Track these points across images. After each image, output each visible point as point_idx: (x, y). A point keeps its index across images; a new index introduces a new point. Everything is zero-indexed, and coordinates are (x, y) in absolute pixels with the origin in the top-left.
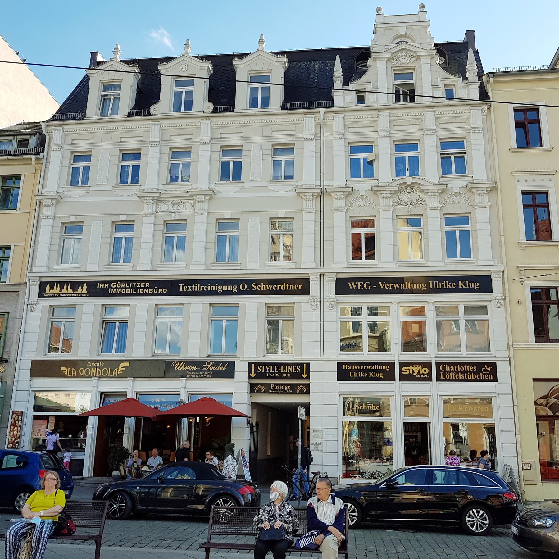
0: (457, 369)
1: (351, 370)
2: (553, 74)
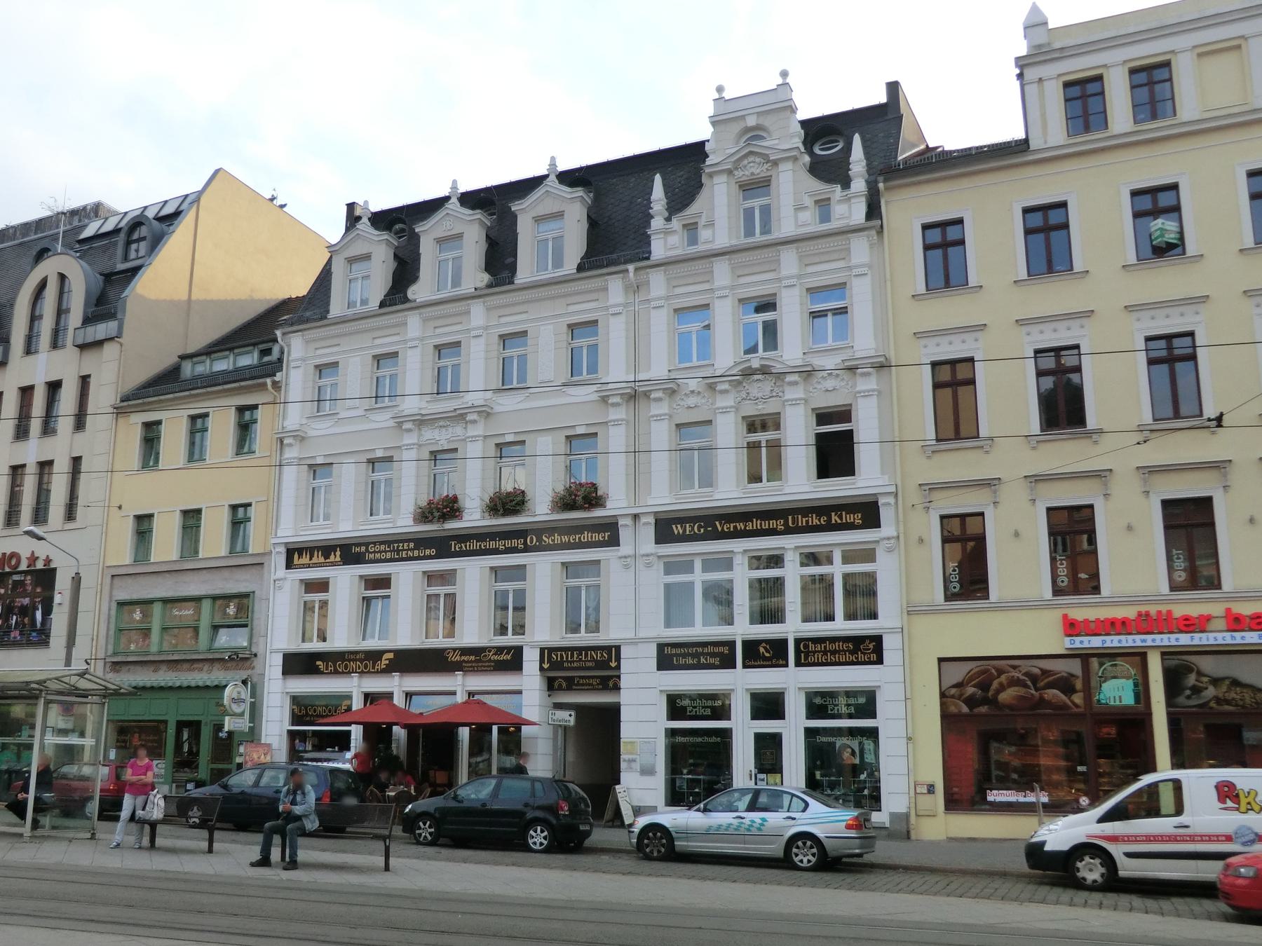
1: (676, 655)
2: (917, 174)
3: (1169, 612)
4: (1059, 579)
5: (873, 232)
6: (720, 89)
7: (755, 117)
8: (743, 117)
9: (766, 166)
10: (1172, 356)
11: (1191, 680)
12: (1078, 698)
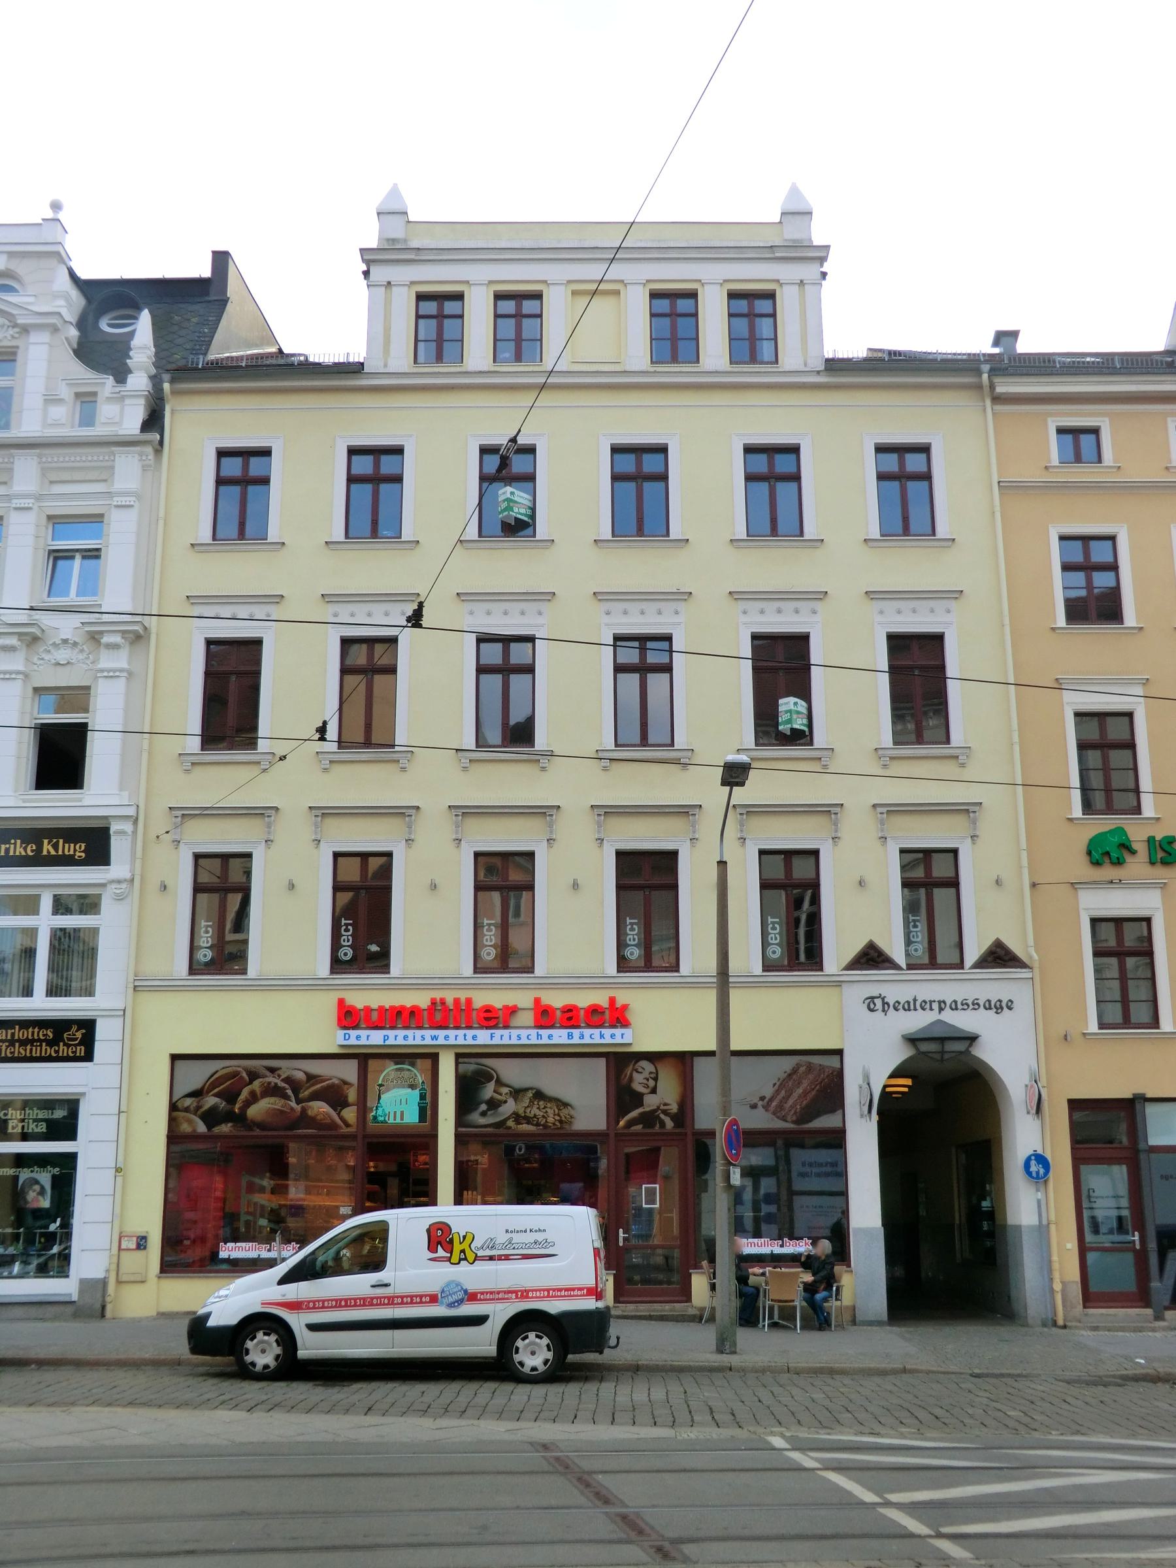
0: (13, 1034)
3: (469, 1001)
5: (149, 450)
9: (11, 332)
11: (489, 1091)
12: (350, 1114)
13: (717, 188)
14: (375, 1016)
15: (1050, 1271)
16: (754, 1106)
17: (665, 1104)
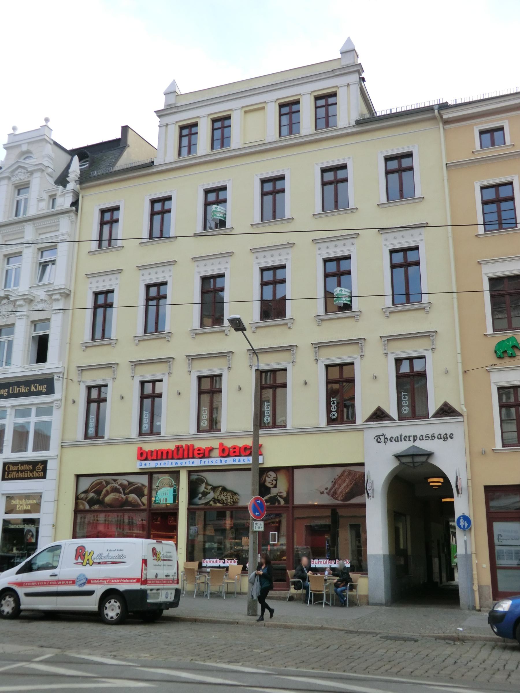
3: (193, 446)
4: (403, 409)
6: (14, 129)
7: (26, 145)
8: (20, 146)
10: (404, 261)
11: (202, 488)
12: (145, 499)
13: (288, 47)
14: (154, 454)
15: (472, 579)
16: (322, 493)
17: (281, 493)
